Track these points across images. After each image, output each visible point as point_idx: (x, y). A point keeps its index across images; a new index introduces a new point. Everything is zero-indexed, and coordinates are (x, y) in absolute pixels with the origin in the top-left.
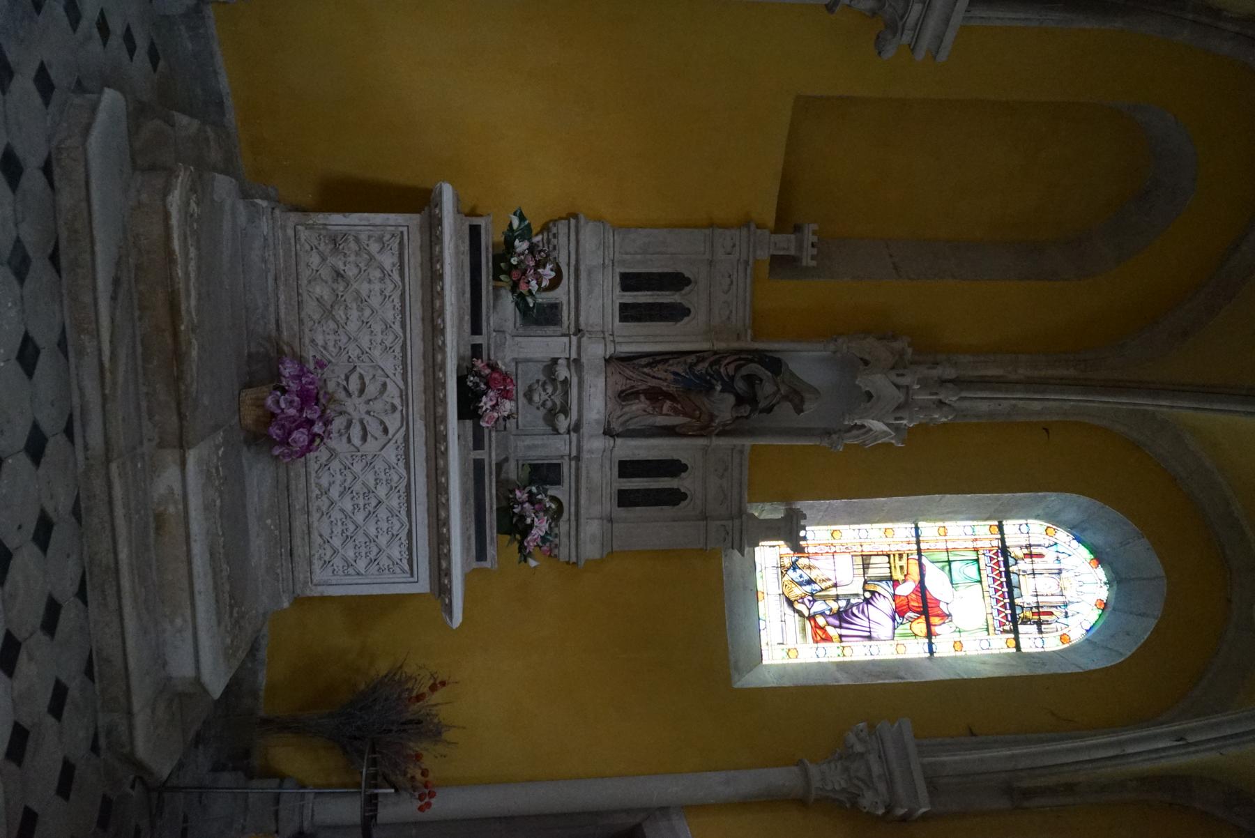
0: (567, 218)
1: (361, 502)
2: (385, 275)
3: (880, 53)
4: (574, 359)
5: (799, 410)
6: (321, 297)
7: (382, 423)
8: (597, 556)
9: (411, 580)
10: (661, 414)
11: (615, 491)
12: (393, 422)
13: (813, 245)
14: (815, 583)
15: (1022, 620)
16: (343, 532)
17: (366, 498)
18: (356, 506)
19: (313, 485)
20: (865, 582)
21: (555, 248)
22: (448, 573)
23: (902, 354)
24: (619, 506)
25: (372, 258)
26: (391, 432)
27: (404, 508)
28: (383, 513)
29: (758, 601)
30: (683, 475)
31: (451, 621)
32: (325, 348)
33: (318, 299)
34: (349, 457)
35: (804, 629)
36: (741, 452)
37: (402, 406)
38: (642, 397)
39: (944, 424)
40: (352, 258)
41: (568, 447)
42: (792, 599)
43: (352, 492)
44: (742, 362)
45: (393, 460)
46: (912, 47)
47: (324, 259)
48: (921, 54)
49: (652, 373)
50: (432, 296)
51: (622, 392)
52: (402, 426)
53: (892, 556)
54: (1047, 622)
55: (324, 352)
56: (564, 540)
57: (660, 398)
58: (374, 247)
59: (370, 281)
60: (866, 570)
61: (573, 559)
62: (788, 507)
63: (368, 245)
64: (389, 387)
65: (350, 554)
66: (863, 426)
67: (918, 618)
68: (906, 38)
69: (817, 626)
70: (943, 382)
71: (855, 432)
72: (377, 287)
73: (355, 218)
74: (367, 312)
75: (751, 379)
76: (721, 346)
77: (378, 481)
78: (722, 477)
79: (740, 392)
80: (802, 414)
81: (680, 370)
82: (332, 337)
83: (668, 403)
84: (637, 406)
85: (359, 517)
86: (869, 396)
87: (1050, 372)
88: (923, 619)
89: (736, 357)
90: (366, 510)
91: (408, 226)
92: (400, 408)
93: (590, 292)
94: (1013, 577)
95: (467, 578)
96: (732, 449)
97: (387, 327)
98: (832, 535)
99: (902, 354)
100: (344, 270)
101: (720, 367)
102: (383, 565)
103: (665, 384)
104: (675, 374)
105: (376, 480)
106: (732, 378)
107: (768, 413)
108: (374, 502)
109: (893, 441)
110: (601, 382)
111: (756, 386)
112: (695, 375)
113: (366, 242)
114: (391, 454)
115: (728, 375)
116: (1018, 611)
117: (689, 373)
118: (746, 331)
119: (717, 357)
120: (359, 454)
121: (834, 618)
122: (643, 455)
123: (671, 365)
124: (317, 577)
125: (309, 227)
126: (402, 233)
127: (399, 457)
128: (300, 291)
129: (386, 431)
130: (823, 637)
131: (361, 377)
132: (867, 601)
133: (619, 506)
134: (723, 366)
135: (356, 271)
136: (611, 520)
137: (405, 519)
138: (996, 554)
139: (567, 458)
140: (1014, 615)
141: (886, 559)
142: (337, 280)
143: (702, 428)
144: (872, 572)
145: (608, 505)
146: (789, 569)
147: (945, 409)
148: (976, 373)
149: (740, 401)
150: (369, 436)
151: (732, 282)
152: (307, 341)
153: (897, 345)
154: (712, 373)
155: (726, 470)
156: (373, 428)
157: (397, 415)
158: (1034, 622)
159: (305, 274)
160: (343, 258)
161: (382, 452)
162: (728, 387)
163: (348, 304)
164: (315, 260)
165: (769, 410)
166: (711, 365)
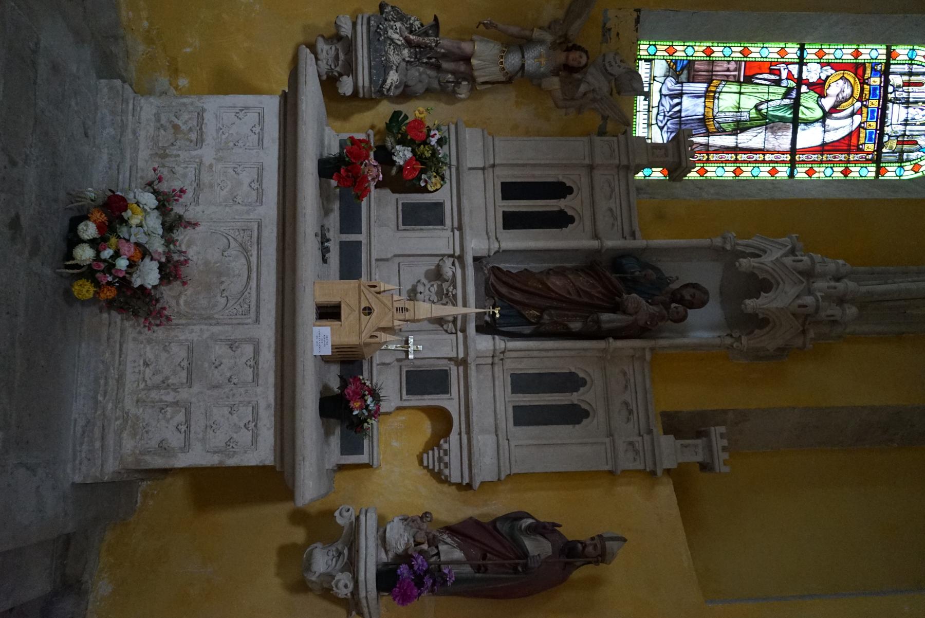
4: (467, 484)
13: (724, 449)
41: (455, 350)
61: (466, 480)
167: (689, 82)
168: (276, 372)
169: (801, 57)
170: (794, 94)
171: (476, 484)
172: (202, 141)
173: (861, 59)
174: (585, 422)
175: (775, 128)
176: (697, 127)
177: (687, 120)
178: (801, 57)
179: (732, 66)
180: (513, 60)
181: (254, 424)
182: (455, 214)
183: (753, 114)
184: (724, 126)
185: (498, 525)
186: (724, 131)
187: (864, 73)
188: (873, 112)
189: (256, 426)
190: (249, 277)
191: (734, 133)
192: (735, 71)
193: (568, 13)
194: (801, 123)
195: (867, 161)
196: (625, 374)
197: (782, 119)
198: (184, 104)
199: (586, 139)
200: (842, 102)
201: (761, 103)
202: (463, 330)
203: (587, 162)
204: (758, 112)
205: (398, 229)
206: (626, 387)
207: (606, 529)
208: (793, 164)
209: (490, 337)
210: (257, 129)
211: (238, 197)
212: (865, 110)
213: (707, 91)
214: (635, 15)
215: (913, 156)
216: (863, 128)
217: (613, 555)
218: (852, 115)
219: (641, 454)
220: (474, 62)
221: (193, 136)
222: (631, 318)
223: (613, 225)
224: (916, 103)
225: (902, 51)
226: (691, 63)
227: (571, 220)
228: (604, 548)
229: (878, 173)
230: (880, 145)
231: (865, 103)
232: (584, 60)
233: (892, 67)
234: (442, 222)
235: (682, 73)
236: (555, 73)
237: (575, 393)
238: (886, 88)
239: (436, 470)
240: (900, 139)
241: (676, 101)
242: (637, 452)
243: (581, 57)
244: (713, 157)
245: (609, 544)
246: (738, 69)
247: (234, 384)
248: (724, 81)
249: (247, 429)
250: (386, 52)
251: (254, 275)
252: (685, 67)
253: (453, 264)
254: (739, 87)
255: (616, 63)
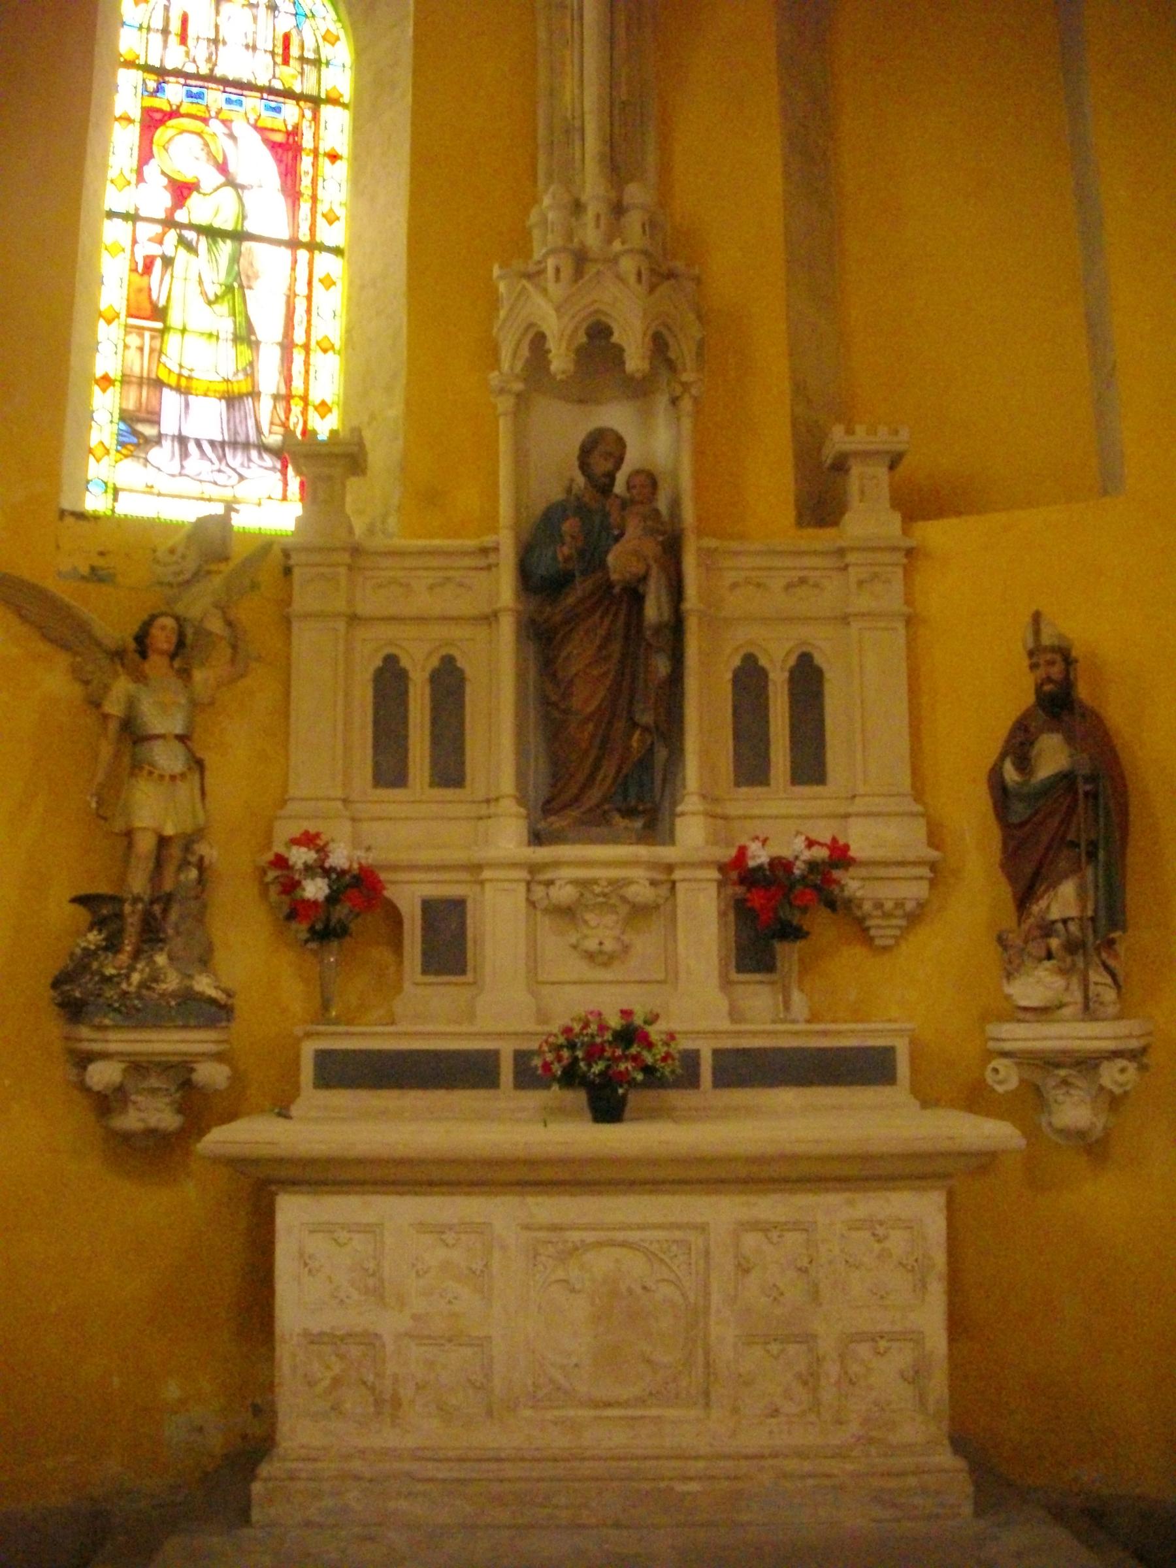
61: (925, 871)
167: (158, 423)
168: (792, 1192)
169: (126, 217)
170: (190, 235)
171: (934, 854)
172: (366, 1333)
173: (136, 115)
174: (819, 660)
175: (250, 273)
176: (242, 413)
177: (229, 429)
178: (126, 217)
179: (134, 340)
180: (168, 758)
181: (878, 1227)
182: (446, 876)
183: (223, 308)
184: (243, 363)
185: (1015, 820)
186: (251, 364)
187: (158, 110)
188: (229, 101)
189: (881, 1223)
190: (623, 1244)
191: (254, 345)
192: (141, 336)
193: (64, 646)
194: (242, 226)
195: (315, 118)
196: (734, 586)
197: (235, 259)
198: (294, 1368)
199: (296, 626)
200: (209, 153)
201: (204, 293)
202: (670, 868)
203: (341, 625)
204: (220, 301)
205: (475, 983)
206: (758, 585)
207: (1018, 640)
208: (313, 246)
209: (679, 821)
210: (343, 1236)
211: (474, 1266)
212: (222, 116)
213: (178, 389)
214: (70, 520)
215: (310, 44)
216: (256, 121)
217: (1061, 636)
218: (232, 136)
219: (877, 569)
220: (169, 831)
221: (355, 1351)
222: (655, 570)
223: (461, 585)
224: (217, 27)
225: (128, 42)
226: (126, 417)
227: (448, 662)
228: (1053, 649)
229: (334, 101)
230: (288, 94)
231: (213, 114)
232: (169, 622)
233: (150, 62)
234: (458, 905)
235: (142, 434)
236: (185, 674)
237: (772, 676)
238: (187, 76)
239: (903, 922)
240: (279, 60)
241: (192, 446)
242: (875, 577)
243: (163, 628)
244: (298, 387)
245: (1046, 640)
246: (140, 330)
247: (811, 1262)
248: (160, 357)
249: (886, 1237)
250: (162, 995)
251: (620, 1236)
252: (130, 426)
253: (549, 883)
254: (172, 331)
255: (177, 563)
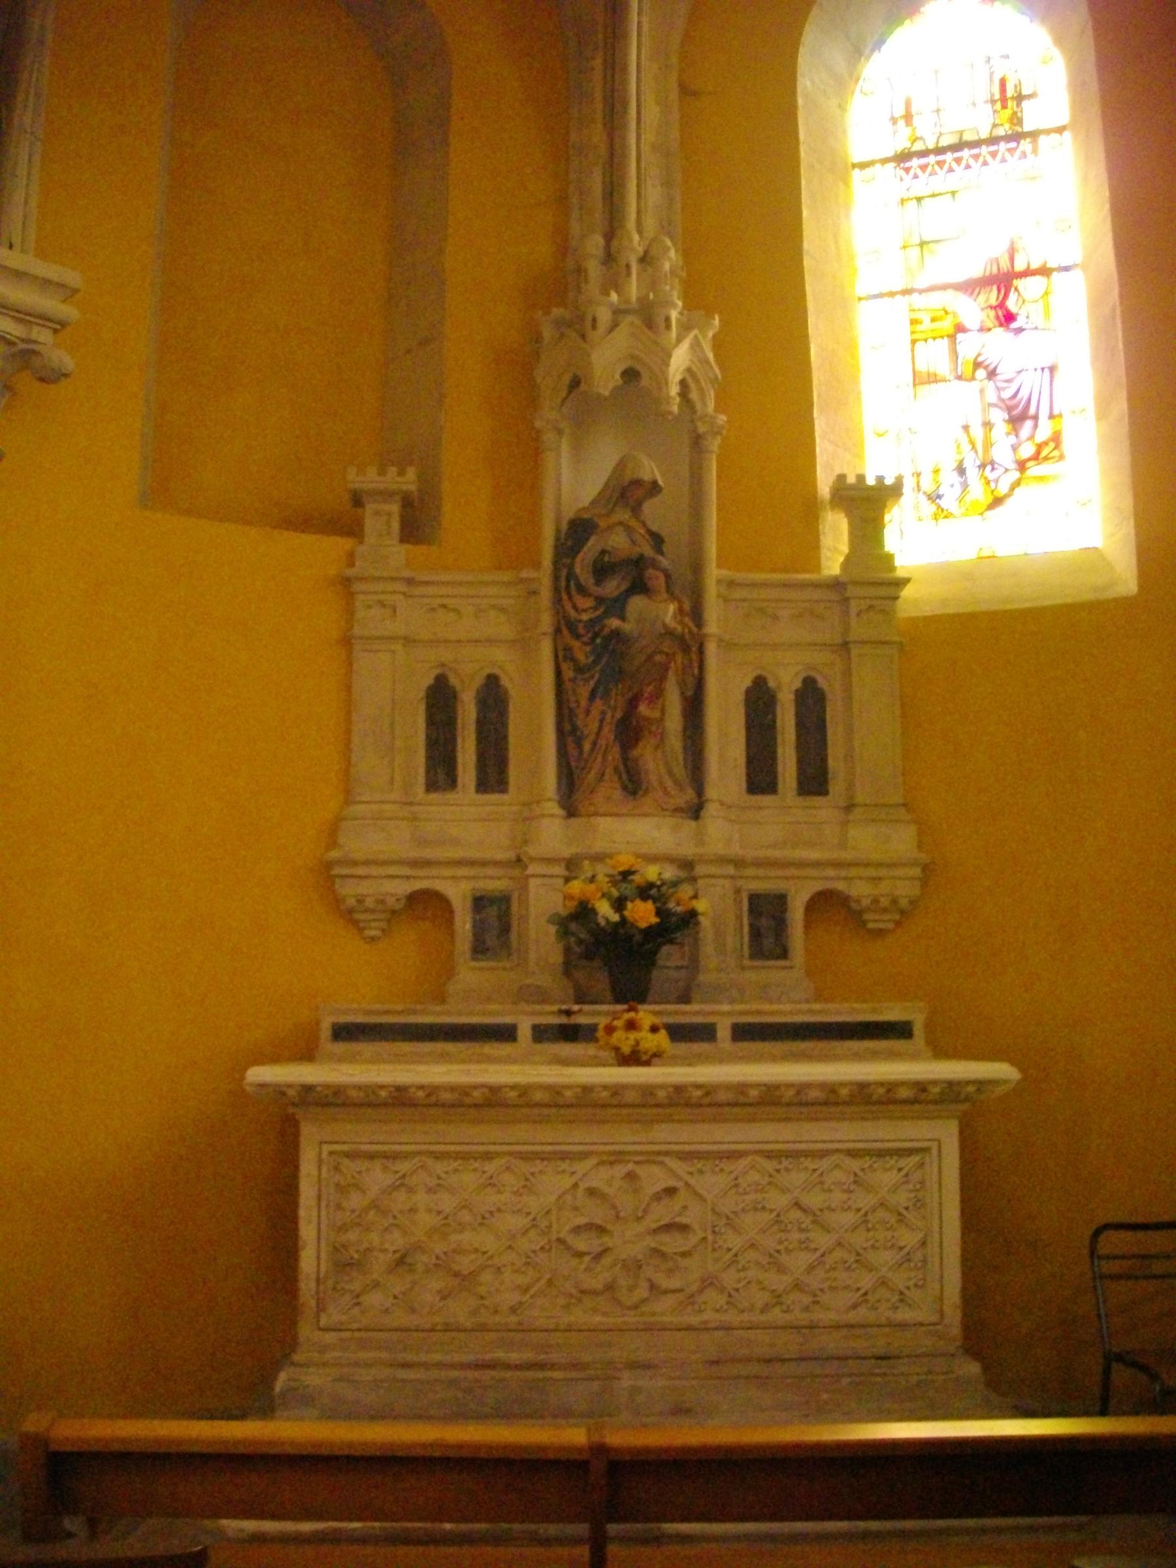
0: (331, 879)
1: (796, 1236)
2: (401, 1184)
3: (66, 375)
5: (654, 488)
6: (439, 1292)
7: (657, 1197)
8: (912, 830)
9: (934, 1152)
10: (662, 720)
11: (800, 801)
12: (654, 1178)
14: (961, 462)
15: (1015, 125)
16: (849, 1268)
17: (789, 1227)
18: (805, 1245)
19: (763, 1318)
20: (959, 378)
21: (382, 902)
22: (921, 1087)
23: (559, 324)
24: (800, 794)
25: (374, 1205)
26: (671, 1183)
27: (808, 1163)
28: (815, 1200)
29: (994, 557)
30: (772, 684)
31: (1006, 1082)
32: (526, 1290)
33: (443, 1298)
34: (716, 1255)
35: (1041, 479)
36: (731, 584)
37: (629, 1161)
38: (635, 753)
39: (686, 253)
40: (375, 1238)
42: (990, 499)
43: (778, 1251)
44: (572, 583)
45: (723, 1180)
46: (58, 327)
47: (376, 1285)
48: (67, 311)
49: (592, 737)
50: (436, 1105)
51: (625, 788)
52: (661, 1163)
53: (916, 336)
54: (1017, 87)
55: (532, 1292)
56: (885, 887)
57: (634, 723)
58: (356, 1201)
59: (413, 1210)
60: (938, 378)
62: (828, 507)
63: (353, 1211)
64: (594, 1184)
65: (885, 1258)
66: (683, 383)
67: (1016, 289)
68: (43, 336)
69: (1036, 457)
70: (609, 258)
71: (694, 395)
72: (421, 1198)
73: (307, 1231)
74: (465, 1216)
75: (602, 570)
76: (546, 621)
77: (759, 1206)
78: (775, 618)
79: (624, 587)
80: (660, 482)
81: (584, 692)
82: (507, 1275)
83: (643, 709)
84: (648, 756)
85: (823, 1240)
86: (631, 375)
87: (598, 94)
88: (1016, 282)
89: (565, 597)
90: (810, 1227)
91: (321, 1143)
92: (630, 1166)
93: (456, 842)
94: (944, 142)
95: (940, 1052)
96: (726, 600)
97: (490, 1183)
98: (881, 436)
99: (559, 324)
100: (395, 1252)
101: (580, 621)
102: (909, 1200)
103: (609, 715)
104: (593, 695)
105: (756, 1209)
106: (600, 600)
107: (663, 541)
108: (796, 1214)
109: (710, 334)
110: (605, 824)
111: (613, 560)
112: (595, 662)
113: (348, 1214)
114: (712, 1182)
115: (595, 608)
116: (1001, 132)
117: (592, 672)
118: (521, 580)
119: (565, 626)
120: (710, 1238)
121: (1021, 427)
122: (737, 752)
123: (578, 702)
124: (924, 1314)
125: (321, 1308)
126: (331, 1153)
127: (717, 1169)
128: (428, 1326)
129: (671, 1191)
130: (1052, 445)
131: (577, 1230)
132: (992, 374)
133: (800, 794)
134: (579, 617)
135: (396, 1234)
136: (849, 808)
137: (825, 1164)
138: (907, 170)
139: (740, 883)
140: (1008, 138)
141: (918, 344)
142: (410, 1265)
143: (686, 649)
144: (943, 367)
145: (823, 809)
146: (939, 507)
147: (654, 252)
148: (600, 205)
149: (640, 587)
150: (677, 1220)
151: (444, 606)
152: (513, 1319)
153: (547, 333)
154: (590, 635)
155: (761, 610)
156: (661, 1213)
157: (642, 1171)
158: (1019, 105)
159: (400, 1318)
160: (375, 1253)
161: (709, 1197)
162: (617, 606)
163: (451, 1247)
164: (374, 1299)
165: (657, 540)
166: (578, 636)
